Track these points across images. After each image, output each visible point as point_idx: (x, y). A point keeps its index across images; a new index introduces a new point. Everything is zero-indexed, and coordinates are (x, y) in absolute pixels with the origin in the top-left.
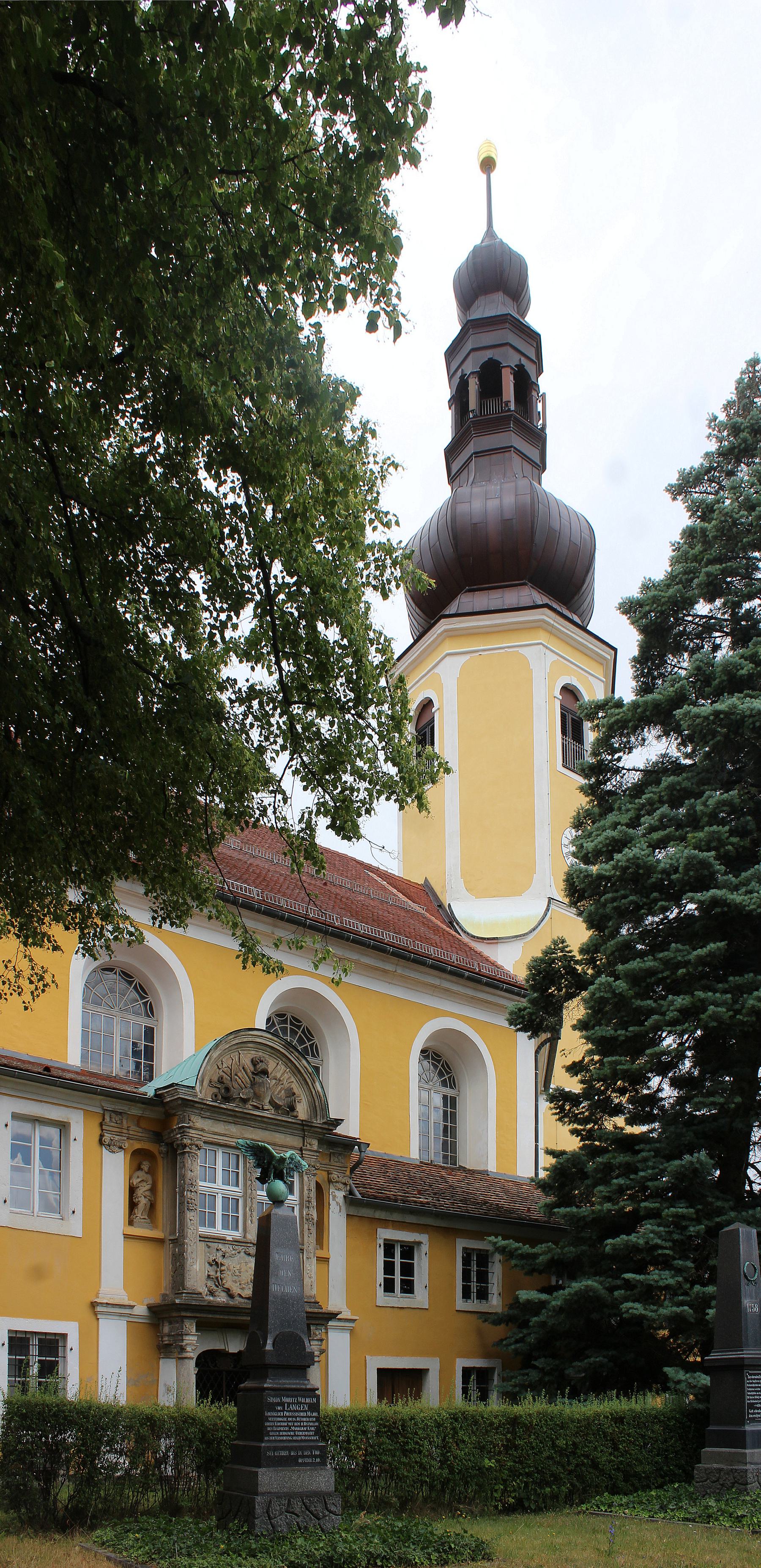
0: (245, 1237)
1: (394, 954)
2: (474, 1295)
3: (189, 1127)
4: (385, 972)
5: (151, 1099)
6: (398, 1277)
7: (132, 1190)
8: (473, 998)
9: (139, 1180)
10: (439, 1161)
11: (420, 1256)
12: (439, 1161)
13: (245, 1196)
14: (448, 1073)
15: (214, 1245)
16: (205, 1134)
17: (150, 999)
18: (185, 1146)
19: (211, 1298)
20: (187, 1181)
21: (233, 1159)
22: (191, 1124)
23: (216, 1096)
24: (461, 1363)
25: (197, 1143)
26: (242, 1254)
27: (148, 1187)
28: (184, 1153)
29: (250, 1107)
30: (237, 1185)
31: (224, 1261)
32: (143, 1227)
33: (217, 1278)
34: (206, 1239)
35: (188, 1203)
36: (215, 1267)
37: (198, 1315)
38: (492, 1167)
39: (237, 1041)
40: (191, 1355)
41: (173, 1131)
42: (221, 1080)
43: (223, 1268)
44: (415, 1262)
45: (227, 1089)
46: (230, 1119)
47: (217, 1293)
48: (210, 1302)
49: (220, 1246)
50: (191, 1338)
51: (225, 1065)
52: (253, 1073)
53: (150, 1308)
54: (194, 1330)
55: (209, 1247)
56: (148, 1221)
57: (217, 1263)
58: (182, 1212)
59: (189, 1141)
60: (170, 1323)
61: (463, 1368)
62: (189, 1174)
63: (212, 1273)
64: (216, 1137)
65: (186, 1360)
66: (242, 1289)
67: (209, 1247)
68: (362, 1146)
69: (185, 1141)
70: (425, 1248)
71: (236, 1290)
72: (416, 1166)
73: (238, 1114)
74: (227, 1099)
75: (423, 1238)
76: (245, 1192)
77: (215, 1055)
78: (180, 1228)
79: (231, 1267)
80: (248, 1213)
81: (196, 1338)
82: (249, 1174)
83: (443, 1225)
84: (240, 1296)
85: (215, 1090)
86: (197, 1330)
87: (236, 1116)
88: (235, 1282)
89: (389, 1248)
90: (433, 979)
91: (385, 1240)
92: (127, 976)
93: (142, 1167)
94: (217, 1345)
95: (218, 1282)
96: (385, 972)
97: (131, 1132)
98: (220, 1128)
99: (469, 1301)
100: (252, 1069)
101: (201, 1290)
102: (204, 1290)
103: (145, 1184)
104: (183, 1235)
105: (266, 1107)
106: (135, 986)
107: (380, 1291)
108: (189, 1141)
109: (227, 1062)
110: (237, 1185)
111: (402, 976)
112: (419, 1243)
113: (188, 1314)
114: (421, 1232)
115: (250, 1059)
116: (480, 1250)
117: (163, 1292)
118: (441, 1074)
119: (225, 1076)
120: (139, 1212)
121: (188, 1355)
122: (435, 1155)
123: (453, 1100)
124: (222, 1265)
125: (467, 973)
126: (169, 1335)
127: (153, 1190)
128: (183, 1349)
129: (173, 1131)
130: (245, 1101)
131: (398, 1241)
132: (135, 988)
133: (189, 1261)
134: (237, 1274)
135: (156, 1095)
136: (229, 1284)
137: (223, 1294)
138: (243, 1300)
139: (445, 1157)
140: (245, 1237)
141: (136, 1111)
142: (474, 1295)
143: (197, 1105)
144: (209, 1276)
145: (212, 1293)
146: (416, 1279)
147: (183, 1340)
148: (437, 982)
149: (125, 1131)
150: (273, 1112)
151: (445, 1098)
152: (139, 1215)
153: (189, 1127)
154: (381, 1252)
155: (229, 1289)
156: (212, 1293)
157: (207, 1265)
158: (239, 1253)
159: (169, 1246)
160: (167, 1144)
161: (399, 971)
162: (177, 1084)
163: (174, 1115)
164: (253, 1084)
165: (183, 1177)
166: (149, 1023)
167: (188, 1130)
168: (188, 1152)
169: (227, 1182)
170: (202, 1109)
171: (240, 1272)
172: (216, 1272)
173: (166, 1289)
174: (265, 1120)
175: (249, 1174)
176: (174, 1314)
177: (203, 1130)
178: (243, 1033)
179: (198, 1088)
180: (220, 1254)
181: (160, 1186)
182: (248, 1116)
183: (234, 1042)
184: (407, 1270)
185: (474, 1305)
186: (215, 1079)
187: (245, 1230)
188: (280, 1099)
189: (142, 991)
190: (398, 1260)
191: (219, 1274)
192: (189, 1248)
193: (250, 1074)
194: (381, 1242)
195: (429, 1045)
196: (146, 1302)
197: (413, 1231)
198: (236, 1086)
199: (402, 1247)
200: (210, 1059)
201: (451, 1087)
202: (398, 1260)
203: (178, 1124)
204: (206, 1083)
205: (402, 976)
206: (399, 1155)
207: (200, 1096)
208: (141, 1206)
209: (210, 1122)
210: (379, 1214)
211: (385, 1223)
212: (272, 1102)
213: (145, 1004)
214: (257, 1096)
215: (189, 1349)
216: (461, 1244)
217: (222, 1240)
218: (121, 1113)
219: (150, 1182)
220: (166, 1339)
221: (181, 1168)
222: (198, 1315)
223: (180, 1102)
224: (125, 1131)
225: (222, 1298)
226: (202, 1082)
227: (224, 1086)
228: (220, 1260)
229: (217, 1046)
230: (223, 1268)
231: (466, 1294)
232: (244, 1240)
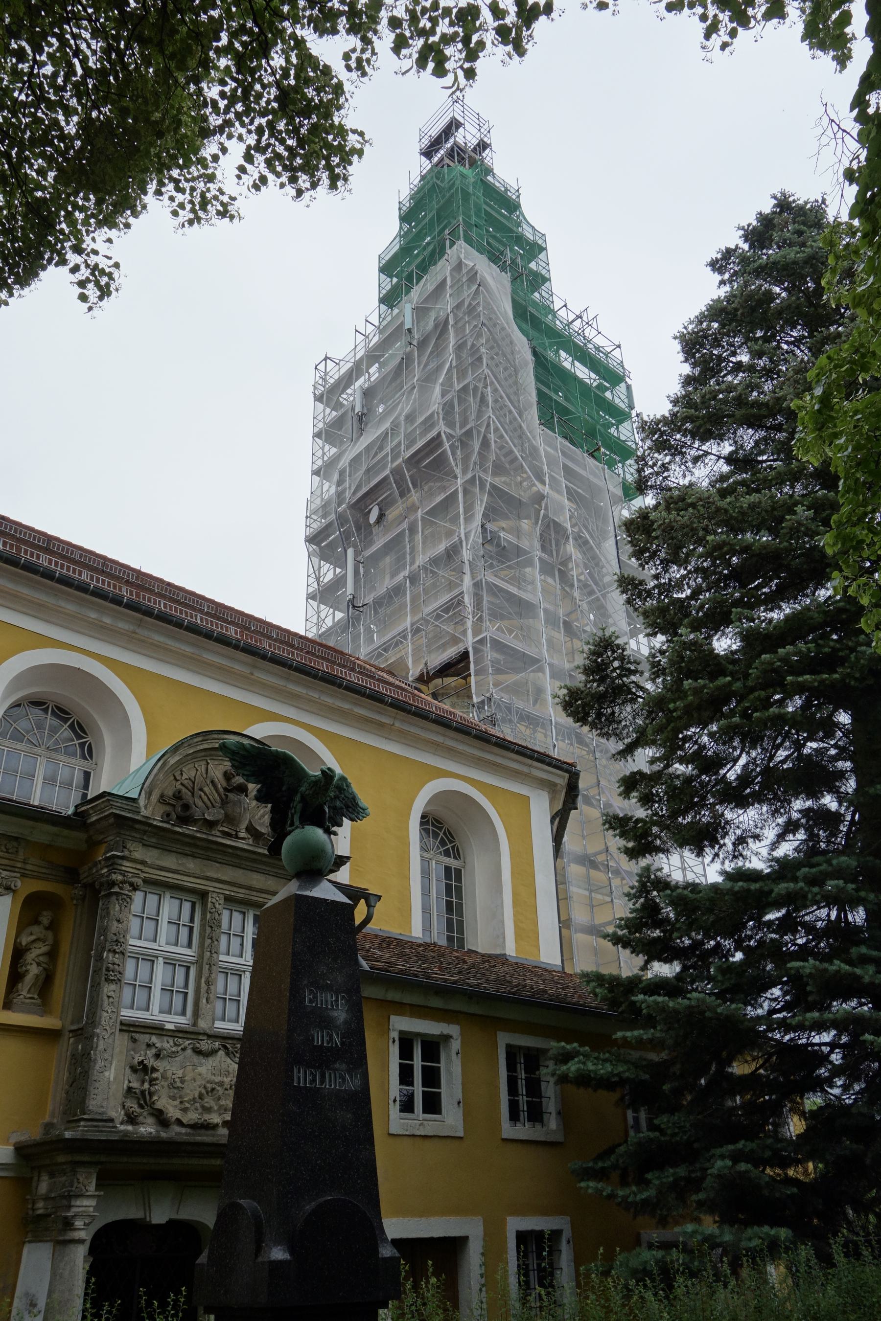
0: (195, 1024)
1: (392, 705)
2: (524, 1116)
3: (123, 858)
4: (381, 725)
5: (68, 817)
6: (418, 1089)
7: (18, 954)
8: (480, 759)
9: (33, 938)
10: (443, 942)
11: (449, 1058)
12: (443, 942)
13: (199, 963)
14: (451, 842)
15: (144, 1038)
16: (146, 870)
17: (89, 739)
18: (113, 884)
19: (130, 1128)
20: (111, 936)
21: (187, 906)
22: (126, 853)
23: (168, 815)
24: (515, 1224)
25: (134, 880)
26: (189, 1052)
27: (44, 949)
28: (110, 894)
29: (218, 834)
30: (189, 945)
31: (158, 1064)
32: (29, 1012)
33: (143, 1092)
34: (130, 1028)
35: (108, 970)
36: (141, 1074)
37: (103, 1159)
38: (511, 949)
39: (206, 746)
40: (82, 1235)
41: (95, 864)
42: (178, 796)
43: (155, 1075)
44: (442, 1065)
45: (186, 807)
46: (187, 850)
47: (141, 1119)
48: (126, 1133)
49: (154, 1039)
50: (86, 1202)
51: (185, 776)
52: (225, 789)
53: (20, 1150)
54: (92, 1188)
55: (134, 1041)
56: (39, 1001)
57: (145, 1066)
58: (96, 986)
59: (120, 878)
60: (52, 1175)
61: (518, 1232)
62: (114, 927)
63: (135, 1085)
64: (163, 873)
65: (72, 1247)
66: (185, 1110)
67: (134, 1041)
68: (372, 899)
69: (114, 876)
70: (456, 1045)
71: (173, 1112)
72: (420, 945)
73: (199, 843)
74: (185, 820)
75: (453, 1030)
76: (201, 955)
77: (173, 761)
78: (89, 1010)
79: (169, 1074)
80: (204, 986)
81: (93, 1202)
82: (208, 930)
83: (480, 1012)
84: (179, 1122)
85: (168, 808)
86: (98, 1187)
87: (196, 846)
88: (173, 1098)
89: (406, 1043)
90: (435, 735)
91: (401, 1032)
92: (61, 713)
93: (41, 919)
94: (130, 1212)
95: (144, 1099)
96: (381, 725)
97: (29, 867)
98: (170, 861)
99: (518, 1124)
100: (225, 784)
101: (113, 1114)
102: (117, 1114)
103: (40, 944)
104: (93, 1021)
105: (242, 835)
106: (72, 724)
107: (394, 1111)
108: (120, 878)
109: (189, 772)
110: (189, 945)
111: (401, 732)
112: (447, 1038)
113: (86, 1159)
114: (449, 1022)
115: (222, 772)
116: (528, 1048)
117: (47, 1119)
118: (443, 843)
119: (184, 790)
120: (24, 989)
121: (77, 1235)
122: (439, 937)
123: (458, 872)
124: (154, 1070)
125: (474, 732)
126: (46, 1198)
127: (52, 954)
128: (68, 1224)
129: (95, 864)
130: (211, 824)
131: (418, 1035)
132: (72, 727)
133: (100, 1063)
134: (179, 1084)
135: (76, 813)
136: (163, 1102)
137: (150, 1120)
138: (183, 1130)
139: (450, 939)
140: (195, 1024)
141: (42, 834)
142: (524, 1116)
143: (137, 826)
144: (130, 1089)
145: (131, 1119)
146: (444, 1090)
147: (69, 1207)
148: (440, 739)
149: (19, 865)
150: (251, 841)
151: (448, 869)
152: (24, 993)
153: (123, 858)
154: (394, 1051)
155: (161, 1112)
156: (131, 1119)
157: (128, 1071)
158: (184, 1049)
159: (67, 1044)
160: (85, 886)
161: (398, 724)
162: (110, 794)
163: (100, 842)
164: (224, 802)
165: (105, 931)
166: (85, 765)
167: (120, 861)
168: (117, 894)
169: (173, 940)
170: (145, 832)
171: (182, 1082)
172: (143, 1082)
173: (53, 1115)
174: (239, 853)
175: (208, 930)
176: (61, 1159)
177: (143, 863)
178: (216, 736)
179: (142, 802)
180: (151, 1052)
181: (65, 947)
182: (214, 847)
183: (201, 747)
184: (432, 1077)
185: (524, 1131)
186: (170, 792)
187: (196, 1014)
188: (262, 825)
189: (79, 729)
190: (418, 1063)
191: (146, 1086)
192: (101, 1042)
193: (221, 790)
194: (395, 1035)
195: (429, 808)
196: (13, 1140)
197: (439, 1020)
198: (200, 803)
199: (423, 1043)
200: (164, 764)
201: (455, 858)
202: (418, 1063)
203: (107, 852)
204: (155, 797)
205: (401, 732)
206: (398, 932)
207: (144, 812)
208: (29, 979)
209: (155, 853)
210: (393, 995)
211: (401, 1008)
212: (250, 829)
213: (82, 745)
214: (230, 819)
215: (79, 1223)
216: (504, 1039)
217: (158, 1030)
218: (16, 839)
219: (50, 940)
220: (40, 1204)
221: (102, 918)
222: (103, 1159)
223: (112, 820)
224: (19, 865)
225: (147, 1129)
226: (149, 794)
227: (181, 803)
228: (151, 1062)
229: (175, 748)
230: (155, 1075)
231: (514, 1116)
232: (192, 1029)
